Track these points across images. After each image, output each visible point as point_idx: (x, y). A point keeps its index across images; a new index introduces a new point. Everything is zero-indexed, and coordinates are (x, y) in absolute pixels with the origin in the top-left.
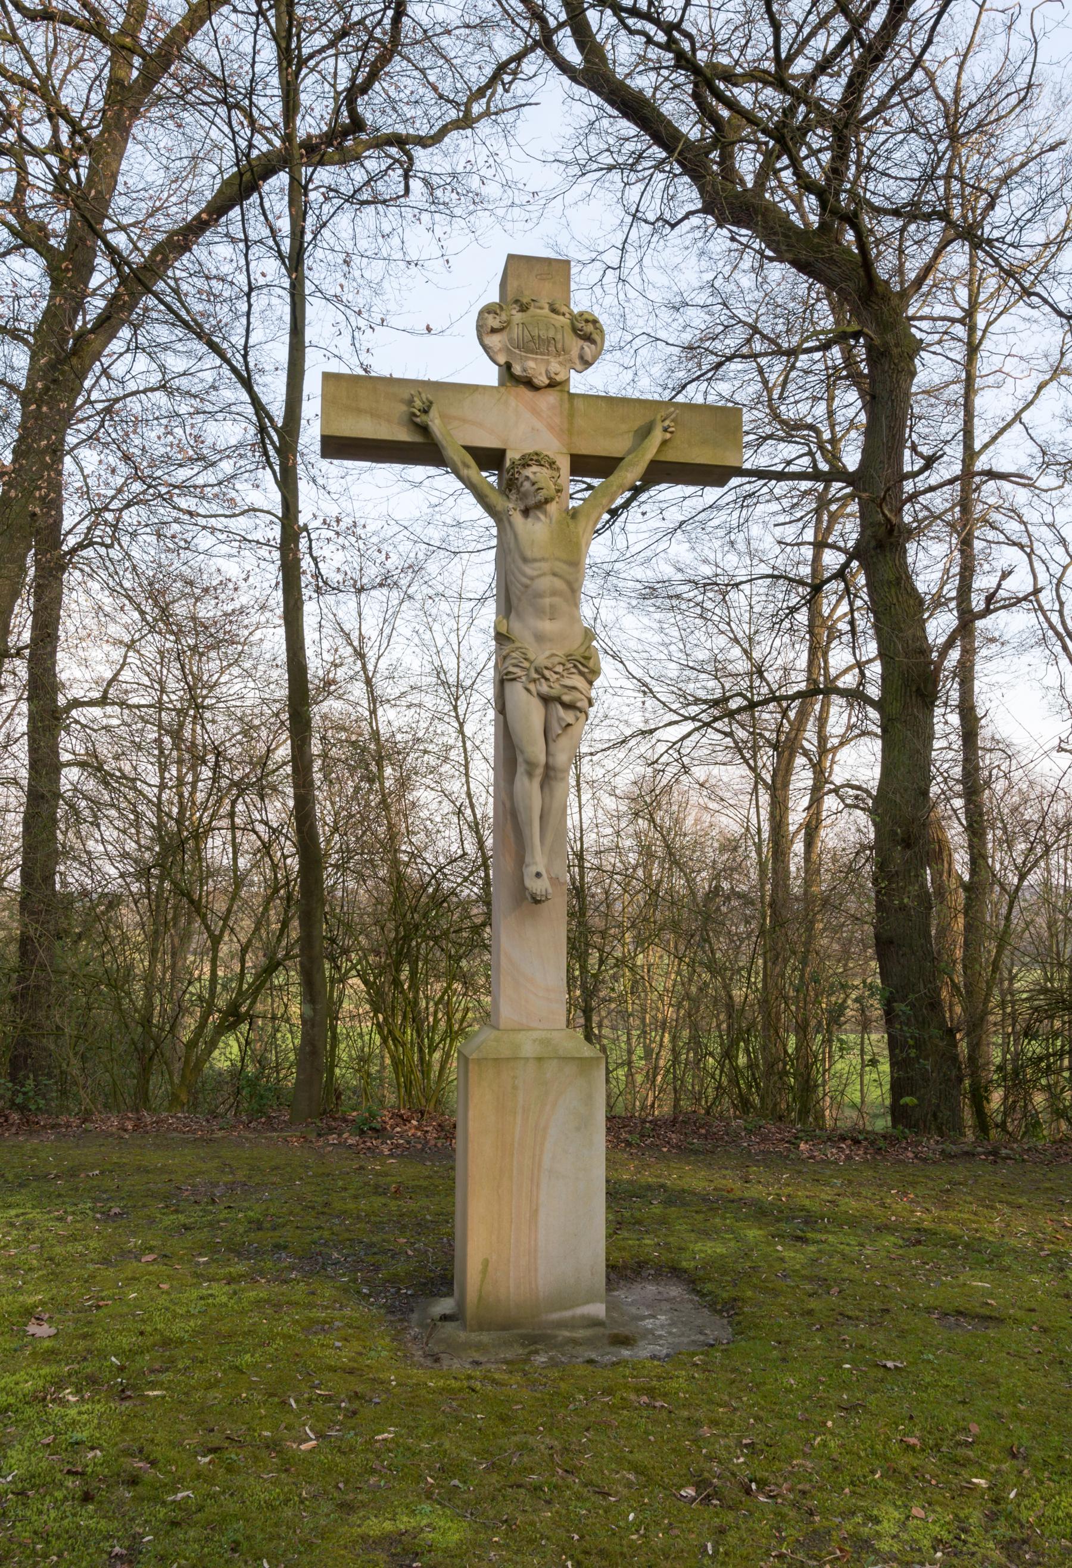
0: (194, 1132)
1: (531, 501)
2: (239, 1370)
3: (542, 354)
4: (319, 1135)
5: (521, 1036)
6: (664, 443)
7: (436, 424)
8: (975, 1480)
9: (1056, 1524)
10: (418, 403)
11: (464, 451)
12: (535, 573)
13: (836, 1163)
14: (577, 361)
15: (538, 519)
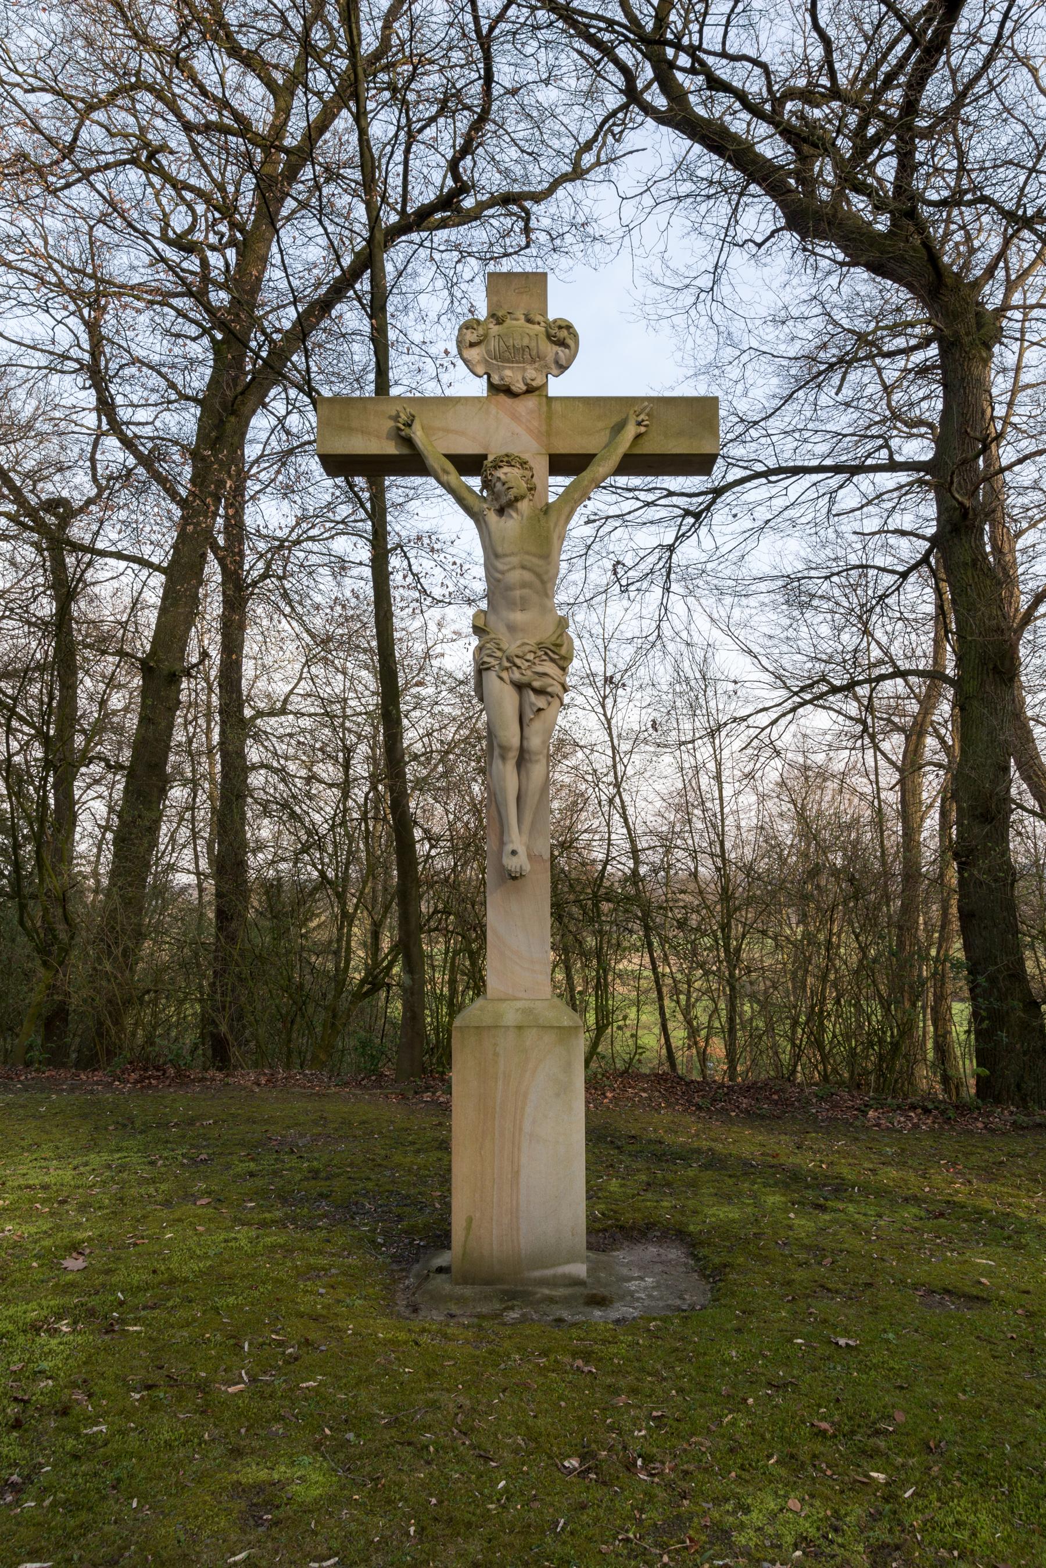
0: (312, 1088)
1: (504, 500)
2: (216, 1310)
3: (518, 362)
4: (416, 1093)
5: (504, 1006)
6: (639, 436)
7: (418, 434)
8: (874, 1474)
9: (942, 1530)
10: (403, 417)
11: (444, 459)
12: (506, 568)
13: (900, 1132)
14: (553, 366)
15: (511, 517)
